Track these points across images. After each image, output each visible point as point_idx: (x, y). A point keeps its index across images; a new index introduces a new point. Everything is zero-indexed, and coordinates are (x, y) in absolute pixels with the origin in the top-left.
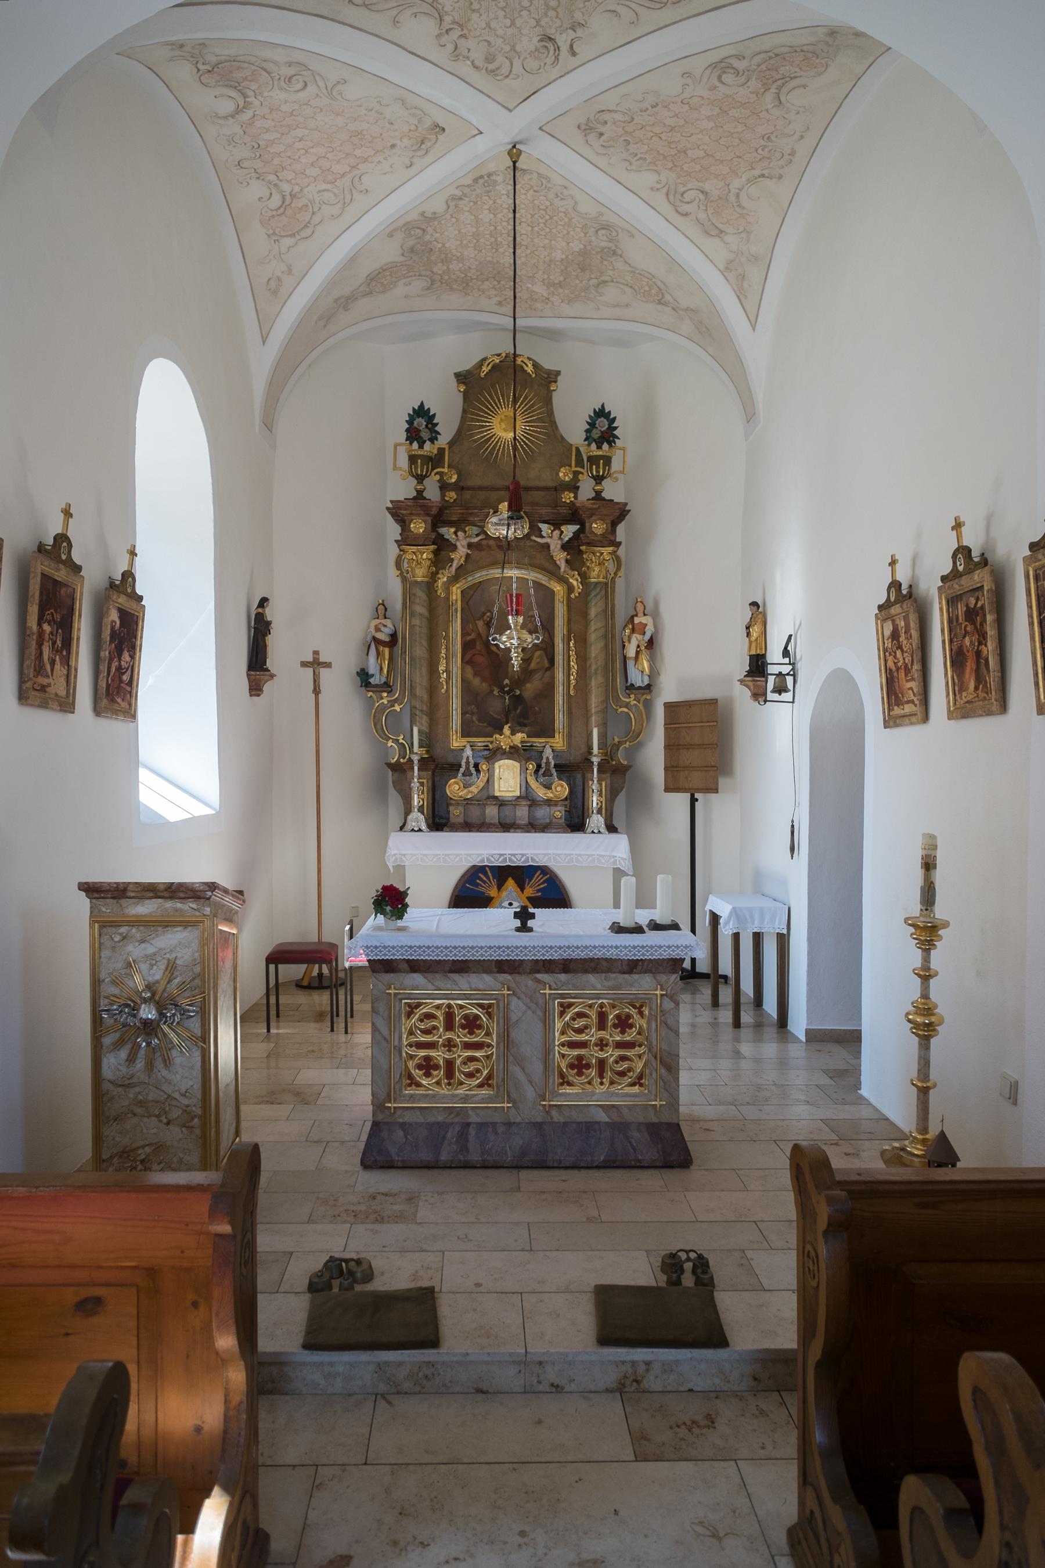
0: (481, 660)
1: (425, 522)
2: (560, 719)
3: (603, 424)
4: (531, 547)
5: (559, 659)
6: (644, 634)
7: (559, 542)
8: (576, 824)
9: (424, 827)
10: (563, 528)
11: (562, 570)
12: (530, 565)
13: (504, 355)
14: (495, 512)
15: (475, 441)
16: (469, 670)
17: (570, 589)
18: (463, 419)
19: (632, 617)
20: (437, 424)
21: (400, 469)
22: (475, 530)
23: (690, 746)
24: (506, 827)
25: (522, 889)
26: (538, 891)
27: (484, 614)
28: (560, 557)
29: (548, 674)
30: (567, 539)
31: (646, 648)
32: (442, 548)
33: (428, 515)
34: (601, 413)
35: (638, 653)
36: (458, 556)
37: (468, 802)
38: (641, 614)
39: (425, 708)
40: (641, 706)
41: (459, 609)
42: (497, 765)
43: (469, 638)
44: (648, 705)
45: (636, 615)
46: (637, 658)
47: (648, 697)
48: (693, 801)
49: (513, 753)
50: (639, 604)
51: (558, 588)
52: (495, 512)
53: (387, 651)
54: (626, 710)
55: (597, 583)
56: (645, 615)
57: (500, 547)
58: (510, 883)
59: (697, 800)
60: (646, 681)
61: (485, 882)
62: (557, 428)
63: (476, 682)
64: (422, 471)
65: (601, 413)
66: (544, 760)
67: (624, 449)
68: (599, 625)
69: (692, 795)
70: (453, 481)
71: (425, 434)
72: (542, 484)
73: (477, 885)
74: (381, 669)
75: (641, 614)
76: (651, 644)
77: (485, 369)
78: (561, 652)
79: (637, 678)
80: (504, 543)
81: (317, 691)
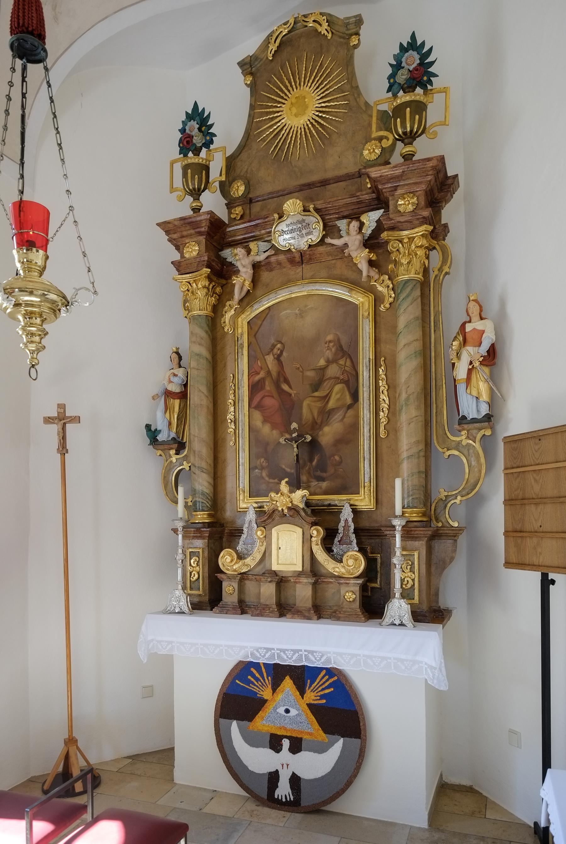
0: (271, 403)
1: (199, 244)
2: (366, 470)
3: (412, 60)
4: (329, 254)
5: (365, 393)
6: (480, 344)
7: (359, 237)
8: (372, 607)
9: (186, 609)
10: (364, 218)
11: (365, 274)
12: (329, 278)
13: (292, 21)
14: (280, 217)
15: (263, 140)
16: (258, 416)
17: (378, 300)
18: (251, 117)
19: (463, 326)
20: (212, 126)
21: (177, 190)
22: (263, 246)
23: (540, 500)
24: (283, 609)
25: (302, 693)
26: (322, 697)
27: (274, 346)
28: (361, 257)
29: (350, 412)
30: (369, 232)
31: (481, 363)
32: (221, 273)
33: (200, 234)
34: (413, 45)
35: (470, 371)
36: (242, 281)
37: (243, 577)
38: (475, 317)
39: (204, 465)
40: (477, 445)
41: (246, 345)
42: (274, 531)
43: (257, 378)
44: (487, 444)
45: (470, 322)
46: (468, 379)
47: (488, 432)
48: (546, 584)
49: (292, 515)
50: (472, 304)
51: (359, 299)
52: (280, 217)
53: (177, 402)
54: (456, 453)
55: (407, 281)
56: (482, 319)
57: (292, 261)
58: (288, 683)
59: (553, 582)
60: (484, 410)
61: (257, 680)
62: (359, 94)
63: (266, 429)
64: (193, 184)
65: (413, 45)
66: (342, 524)
67: (445, 91)
68: (410, 338)
69: (544, 576)
70: (241, 193)
71: (198, 140)
72: (342, 172)
73: (249, 682)
74: (170, 424)
75: (475, 317)
76: (492, 357)
77: (273, 47)
78: (366, 382)
79: (470, 407)
80: (297, 256)
81: (63, 449)
